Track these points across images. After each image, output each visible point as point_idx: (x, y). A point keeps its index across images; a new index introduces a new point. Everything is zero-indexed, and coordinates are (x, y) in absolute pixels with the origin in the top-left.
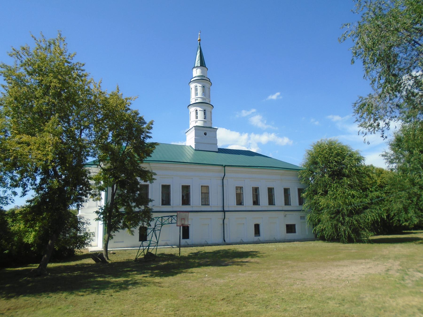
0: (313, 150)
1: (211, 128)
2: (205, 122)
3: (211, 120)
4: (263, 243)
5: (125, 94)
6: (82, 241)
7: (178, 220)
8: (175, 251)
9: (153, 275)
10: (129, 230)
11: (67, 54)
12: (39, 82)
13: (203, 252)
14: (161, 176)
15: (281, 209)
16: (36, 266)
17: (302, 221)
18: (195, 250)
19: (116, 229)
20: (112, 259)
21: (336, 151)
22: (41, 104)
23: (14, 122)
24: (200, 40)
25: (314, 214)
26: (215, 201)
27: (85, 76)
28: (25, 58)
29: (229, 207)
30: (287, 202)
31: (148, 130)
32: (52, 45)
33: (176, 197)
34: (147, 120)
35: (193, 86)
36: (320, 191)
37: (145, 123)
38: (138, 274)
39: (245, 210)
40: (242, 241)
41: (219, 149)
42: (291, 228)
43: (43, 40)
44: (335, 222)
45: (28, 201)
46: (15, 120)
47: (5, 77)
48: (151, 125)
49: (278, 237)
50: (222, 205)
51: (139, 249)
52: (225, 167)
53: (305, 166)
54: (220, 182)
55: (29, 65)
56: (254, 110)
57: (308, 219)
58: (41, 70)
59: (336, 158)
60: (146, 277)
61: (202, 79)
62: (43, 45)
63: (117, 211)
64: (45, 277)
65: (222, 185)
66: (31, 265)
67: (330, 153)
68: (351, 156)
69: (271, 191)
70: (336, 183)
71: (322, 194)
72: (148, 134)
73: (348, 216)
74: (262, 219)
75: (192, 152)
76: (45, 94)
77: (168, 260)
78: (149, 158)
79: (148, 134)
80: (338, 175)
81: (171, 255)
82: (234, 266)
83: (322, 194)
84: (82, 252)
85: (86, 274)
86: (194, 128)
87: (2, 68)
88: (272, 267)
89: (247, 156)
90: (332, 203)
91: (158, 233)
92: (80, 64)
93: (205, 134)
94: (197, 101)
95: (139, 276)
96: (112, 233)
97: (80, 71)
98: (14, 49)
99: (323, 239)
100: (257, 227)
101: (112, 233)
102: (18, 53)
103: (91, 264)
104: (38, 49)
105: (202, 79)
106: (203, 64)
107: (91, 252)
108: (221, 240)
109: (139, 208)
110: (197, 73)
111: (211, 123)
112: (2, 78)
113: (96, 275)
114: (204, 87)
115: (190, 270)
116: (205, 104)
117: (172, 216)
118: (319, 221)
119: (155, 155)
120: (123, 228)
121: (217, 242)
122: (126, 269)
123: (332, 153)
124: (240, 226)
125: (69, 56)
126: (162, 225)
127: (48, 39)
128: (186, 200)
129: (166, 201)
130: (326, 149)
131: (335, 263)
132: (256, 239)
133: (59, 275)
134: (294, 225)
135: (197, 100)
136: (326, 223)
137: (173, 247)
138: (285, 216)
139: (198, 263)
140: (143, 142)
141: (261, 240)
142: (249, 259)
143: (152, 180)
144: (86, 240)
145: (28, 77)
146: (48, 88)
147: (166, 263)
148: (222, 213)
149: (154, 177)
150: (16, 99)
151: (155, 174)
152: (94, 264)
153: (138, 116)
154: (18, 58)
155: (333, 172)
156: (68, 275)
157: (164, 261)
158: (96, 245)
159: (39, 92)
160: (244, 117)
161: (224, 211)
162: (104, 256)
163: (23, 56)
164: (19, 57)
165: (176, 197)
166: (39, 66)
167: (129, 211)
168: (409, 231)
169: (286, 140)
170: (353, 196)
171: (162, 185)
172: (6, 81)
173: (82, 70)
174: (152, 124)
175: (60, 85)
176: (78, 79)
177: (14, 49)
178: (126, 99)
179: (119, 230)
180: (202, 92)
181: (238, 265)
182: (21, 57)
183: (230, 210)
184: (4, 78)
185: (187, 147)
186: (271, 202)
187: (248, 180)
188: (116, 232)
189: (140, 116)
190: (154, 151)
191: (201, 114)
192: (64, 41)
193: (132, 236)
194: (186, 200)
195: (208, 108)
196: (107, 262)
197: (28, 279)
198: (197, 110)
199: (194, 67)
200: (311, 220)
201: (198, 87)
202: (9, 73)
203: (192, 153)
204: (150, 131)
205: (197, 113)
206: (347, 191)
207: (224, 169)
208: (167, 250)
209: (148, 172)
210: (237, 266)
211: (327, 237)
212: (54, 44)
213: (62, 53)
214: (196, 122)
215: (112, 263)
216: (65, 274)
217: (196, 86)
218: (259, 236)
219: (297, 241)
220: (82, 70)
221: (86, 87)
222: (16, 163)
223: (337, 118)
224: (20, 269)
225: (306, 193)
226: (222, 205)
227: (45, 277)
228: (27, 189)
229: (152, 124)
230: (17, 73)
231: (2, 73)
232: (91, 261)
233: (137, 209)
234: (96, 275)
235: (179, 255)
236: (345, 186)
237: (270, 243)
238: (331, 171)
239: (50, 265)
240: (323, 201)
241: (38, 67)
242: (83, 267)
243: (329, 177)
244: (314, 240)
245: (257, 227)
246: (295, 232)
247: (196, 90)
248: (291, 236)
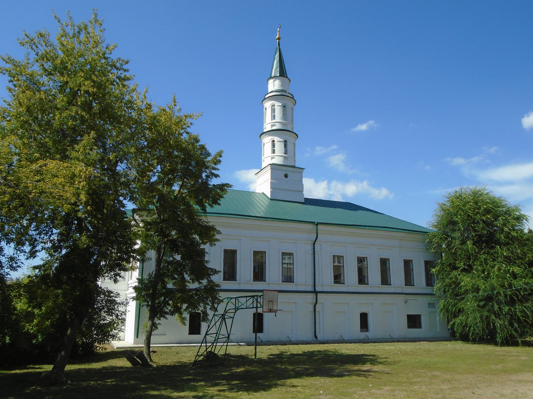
0: (448, 204)
1: (294, 167)
2: (285, 158)
3: (295, 156)
4: (374, 342)
5: (184, 108)
6: (106, 332)
7: (265, 302)
8: (247, 350)
9: (234, 389)
10: (181, 317)
11: (104, 45)
12: (60, 86)
13: (289, 353)
14: (230, 236)
16: (40, 368)
17: (431, 310)
18: (275, 350)
19: (163, 314)
20: (157, 360)
21: (485, 206)
22: (66, 117)
23: (24, 144)
24: (279, 39)
25: (451, 301)
26: (302, 277)
27: (128, 79)
28: (42, 50)
29: (322, 286)
30: (409, 280)
31: (213, 166)
32: (83, 31)
33: (245, 268)
34: (213, 150)
35: (268, 105)
36: (461, 265)
37: (209, 155)
38: (210, 387)
40: (341, 339)
41: (306, 199)
42: (414, 321)
43: (70, 24)
44: (486, 313)
45: (35, 268)
46: (26, 141)
47: (11, 76)
48: (218, 158)
49: (396, 335)
51: (227, 345)
52: (317, 225)
53: (436, 226)
54: (310, 247)
55: (47, 59)
56: (335, 147)
57: (442, 306)
58: (65, 68)
59: (484, 215)
60: (223, 391)
61: (282, 95)
62: (70, 31)
63: (164, 287)
64: (65, 387)
65: (312, 252)
66: (31, 366)
67: (476, 208)
68: (508, 212)
69: (384, 263)
70: (484, 253)
71: (464, 270)
72: (214, 171)
73: (507, 304)
74: (374, 306)
75: (267, 202)
76: (70, 103)
77: (243, 365)
78: (216, 208)
79: (214, 171)
80: (486, 242)
81: (241, 357)
82: (354, 377)
83: (464, 270)
84: (105, 349)
85: (125, 383)
86: (269, 167)
87: (7, 62)
88: (415, 380)
89: (347, 211)
90: (481, 284)
91: (229, 321)
92: (123, 61)
93: (286, 176)
94: (274, 128)
95: (212, 389)
96: (157, 321)
97: (121, 72)
98: (26, 35)
99: (465, 338)
100: (364, 317)
101: (157, 321)
102: (32, 40)
103: (127, 368)
104: (63, 36)
105: (282, 95)
106: (283, 73)
107: (117, 348)
108: (310, 336)
109: (200, 283)
110: (274, 85)
111: (295, 161)
112: (7, 78)
113: (143, 386)
115: (289, 381)
116: (286, 132)
117: (253, 297)
118: (460, 311)
119: (226, 204)
120: (172, 314)
121: (305, 339)
122: (185, 378)
123: (479, 208)
124: (338, 315)
125: (107, 48)
126: (236, 309)
127: (77, 23)
128: (259, 274)
129: (230, 274)
130: (470, 202)
131: (514, 377)
132: (363, 335)
133: (85, 384)
134: (419, 316)
135: (274, 125)
136: (471, 314)
137: (240, 345)
138: (406, 302)
139: (293, 370)
140: (205, 184)
141: (293, 340)
142: (367, 367)
143: (212, 241)
144: (112, 330)
145: (45, 79)
146: (74, 94)
148: (312, 296)
149: (217, 237)
150: (28, 110)
151: (219, 232)
152: (130, 368)
153: (199, 144)
154: (32, 48)
155: (480, 236)
156: (99, 384)
157: (238, 366)
158: (127, 337)
159: (61, 100)
160: (317, 158)
161: (315, 292)
162: (146, 355)
163: (39, 46)
164: (34, 47)
165: (245, 268)
166: (62, 62)
167: (182, 289)
169: (384, 192)
170: (514, 276)
171: (224, 250)
172: (11, 83)
173: (125, 71)
174: (221, 156)
175: (95, 89)
176: (117, 83)
177: (26, 35)
178: (186, 116)
179: (167, 316)
180: (281, 114)
181: (359, 375)
182: (37, 47)
183: (324, 290)
184: (10, 78)
185: (259, 196)
186: (385, 280)
187: (351, 246)
188: (162, 318)
189: (200, 143)
190: (225, 196)
191: (279, 147)
192: (101, 24)
193: (183, 326)
194: (259, 274)
195: (290, 138)
196: (151, 366)
197: (39, 388)
198: (273, 141)
199: (271, 78)
200: (447, 311)
201: (276, 107)
202: (16, 72)
203: (267, 203)
204: (218, 166)
205: (274, 145)
206: (504, 266)
207: (315, 228)
208: (234, 350)
209: (212, 228)
210: (357, 378)
211: (472, 336)
212: (85, 29)
213: (97, 44)
214: (272, 158)
215: (157, 367)
216: (92, 383)
217: (274, 105)
218: (368, 331)
219: (424, 341)
220: (125, 71)
221: (127, 98)
222: (25, 205)
223: (459, 161)
224: (18, 371)
225: (438, 268)
226: (312, 284)
227: (65, 387)
228: (37, 248)
229: (221, 156)
230: (29, 71)
231: (7, 71)
232: (124, 363)
233: (196, 285)
234: (143, 386)
235: (254, 357)
236: (500, 259)
237: (384, 342)
238: (476, 235)
239: (69, 368)
240: (466, 281)
241: (61, 64)
242: (116, 372)
243: (474, 244)
244: (450, 340)
245: (364, 317)
246: (420, 327)
247: (273, 111)
248: (414, 332)
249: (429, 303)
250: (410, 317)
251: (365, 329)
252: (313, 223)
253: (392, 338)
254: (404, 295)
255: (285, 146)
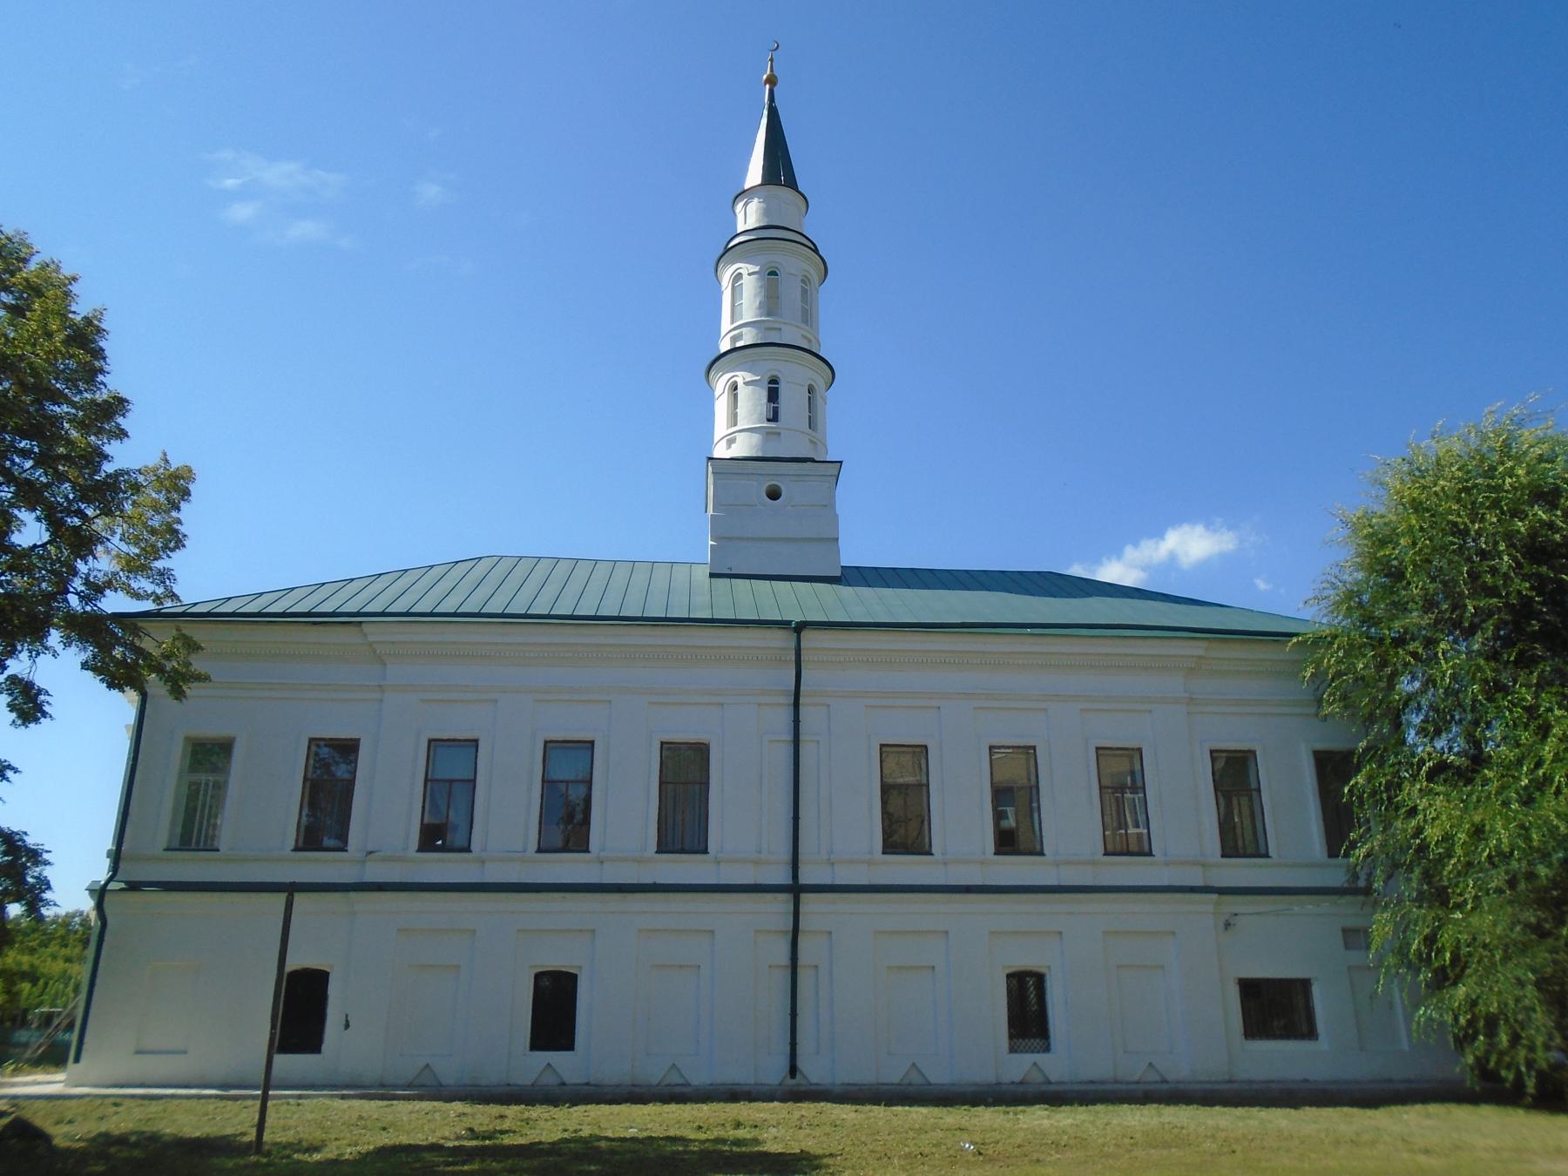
2: (768, 435)
15: (1195, 878)
17: (1354, 957)
26: (743, 826)
30: (1240, 835)
39: (942, 882)
40: (675, 1079)
42: (1273, 1007)
49: (1181, 1068)
50: (785, 854)
65: (790, 737)
74: (1074, 950)
93: (774, 494)
106: (779, 168)
108: (773, 1071)
114: (773, 273)
132: (535, 1066)
134: (1305, 984)
147: (476, 1166)
148: (782, 902)
161: (796, 889)
168: (1239, 831)
183: (838, 882)
186: (1125, 833)
191: (751, 403)
246: (1311, 1034)
248: (1277, 1058)
249: (1345, 931)
250: (1251, 990)
251: (1037, 1042)
252: (783, 624)
253: (564, 1084)
254: (1214, 897)
255: (773, 395)
